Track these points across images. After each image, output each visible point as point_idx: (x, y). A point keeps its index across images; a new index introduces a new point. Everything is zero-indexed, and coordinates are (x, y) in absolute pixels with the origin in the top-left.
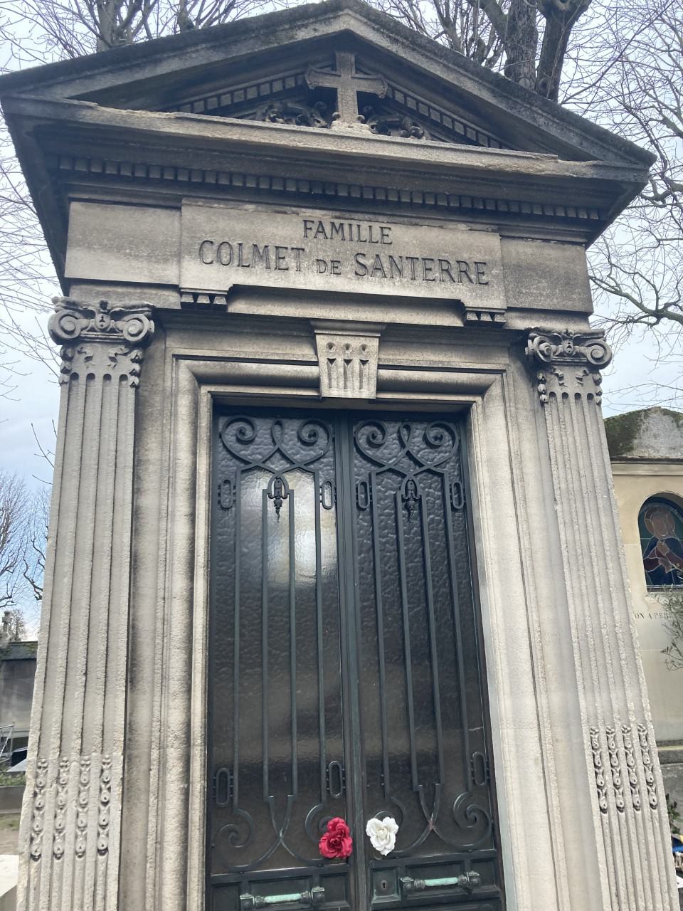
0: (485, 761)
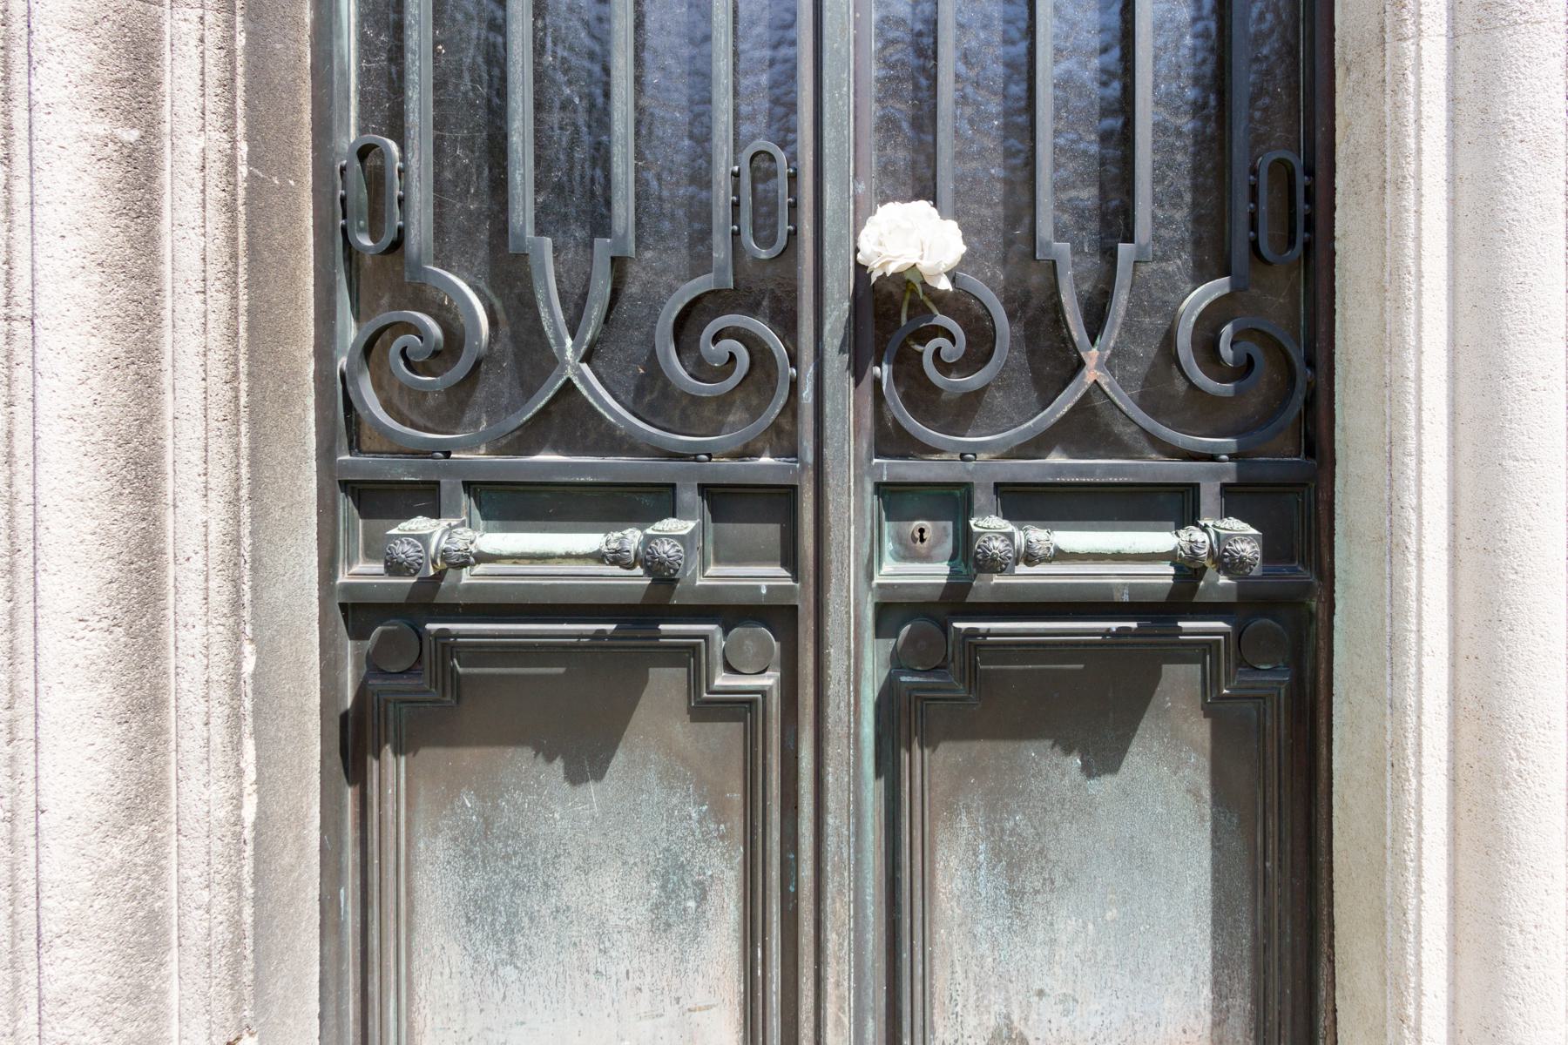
0: (1301, 180)
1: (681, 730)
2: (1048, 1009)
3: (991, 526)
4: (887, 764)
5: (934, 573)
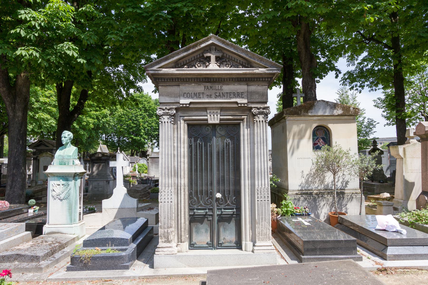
1: (207, 221)
2: (226, 237)
3: (223, 210)
4: (218, 224)
5: (220, 213)
